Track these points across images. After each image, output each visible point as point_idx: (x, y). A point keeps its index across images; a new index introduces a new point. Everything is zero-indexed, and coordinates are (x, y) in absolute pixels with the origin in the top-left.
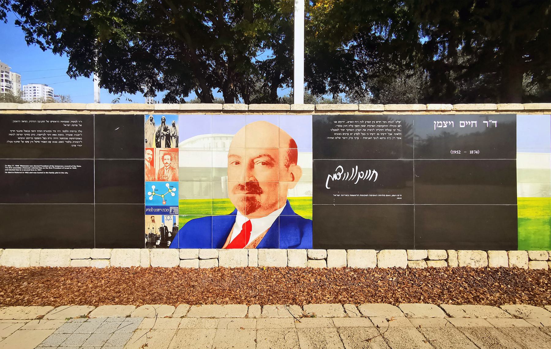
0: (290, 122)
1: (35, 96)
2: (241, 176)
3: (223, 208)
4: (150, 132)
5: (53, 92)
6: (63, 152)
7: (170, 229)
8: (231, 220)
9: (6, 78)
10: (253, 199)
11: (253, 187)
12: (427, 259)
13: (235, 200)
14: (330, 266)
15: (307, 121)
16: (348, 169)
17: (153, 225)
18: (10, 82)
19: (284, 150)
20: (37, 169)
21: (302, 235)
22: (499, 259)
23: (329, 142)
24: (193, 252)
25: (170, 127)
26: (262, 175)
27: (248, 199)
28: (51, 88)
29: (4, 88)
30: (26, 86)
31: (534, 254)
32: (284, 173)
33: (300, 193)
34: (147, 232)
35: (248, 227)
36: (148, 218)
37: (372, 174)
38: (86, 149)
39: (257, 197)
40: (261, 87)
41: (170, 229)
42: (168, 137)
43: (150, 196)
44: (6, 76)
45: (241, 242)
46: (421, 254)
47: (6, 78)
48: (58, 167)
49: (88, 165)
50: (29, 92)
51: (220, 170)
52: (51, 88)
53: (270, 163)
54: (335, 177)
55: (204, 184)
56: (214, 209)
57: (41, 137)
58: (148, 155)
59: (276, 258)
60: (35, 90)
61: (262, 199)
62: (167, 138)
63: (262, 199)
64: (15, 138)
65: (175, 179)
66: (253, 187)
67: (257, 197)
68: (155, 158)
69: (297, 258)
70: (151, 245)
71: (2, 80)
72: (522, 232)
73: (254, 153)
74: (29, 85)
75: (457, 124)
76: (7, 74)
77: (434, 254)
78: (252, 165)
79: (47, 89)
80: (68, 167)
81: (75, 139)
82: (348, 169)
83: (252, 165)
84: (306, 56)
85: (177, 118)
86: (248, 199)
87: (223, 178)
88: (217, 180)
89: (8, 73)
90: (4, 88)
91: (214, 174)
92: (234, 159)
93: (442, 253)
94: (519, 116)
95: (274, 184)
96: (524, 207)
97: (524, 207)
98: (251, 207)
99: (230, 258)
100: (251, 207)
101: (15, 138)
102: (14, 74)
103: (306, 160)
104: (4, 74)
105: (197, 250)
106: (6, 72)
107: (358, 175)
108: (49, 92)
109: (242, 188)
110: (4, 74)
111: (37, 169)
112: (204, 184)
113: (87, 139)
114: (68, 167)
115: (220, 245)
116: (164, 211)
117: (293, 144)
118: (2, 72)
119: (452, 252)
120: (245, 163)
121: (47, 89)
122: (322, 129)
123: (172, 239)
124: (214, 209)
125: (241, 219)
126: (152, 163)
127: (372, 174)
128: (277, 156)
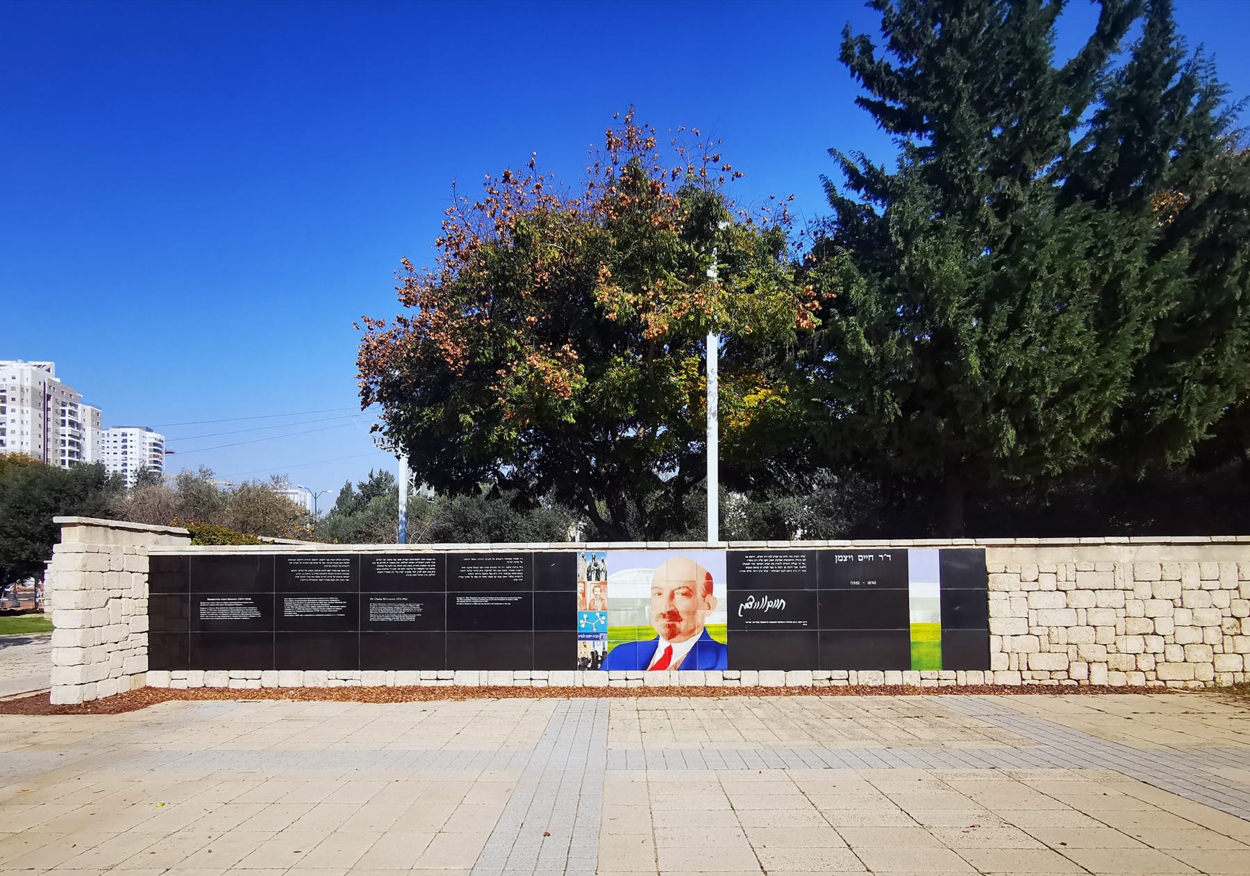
0: (705, 559)
1: (125, 453)
2: (663, 606)
3: (648, 635)
4: (582, 567)
5: (164, 445)
6: (505, 586)
7: (600, 654)
8: (654, 645)
9: (72, 418)
10: (674, 626)
11: (673, 616)
12: (830, 679)
13: (659, 627)
14: (743, 685)
15: (722, 555)
16: (758, 599)
17: (584, 650)
18: (79, 426)
19: (701, 581)
20: (484, 600)
21: (717, 658)
22: (894, 677)
23: (741, 577)
24: (621, 674)
25: (600, 563)
26: (681, 604)
27: (669, 626)
28: (158, 436)
29: (67, 438)
30: (105, 432)
31: (925, 673)
32: (701, 603)
33: (716, 619)
34: (580, 656)
35: (669, 651)
36: (580, 643)
37: (780, 603)
38: (525, 584)
39: (677, 624)
40: (677, 521)
41: (600, 654)
42: (598, 572)
43: (582, 623)
44: (71, 412)
45: (664, 664)
46: (825, 674)
47: (72, 418)
48: (502, 599)
49: (527, 597)
50: (112, 444)
51: (644, 600)
52: (158, 436)
53: (689, 594)
54: (747, 606)
55: (630, 613)
56: (639, 635)
57: (488, 573)
58: (580, 587)
59: (696, 678)
60: (125, 441)
61: (681, 626)
62: (596, 573)
63: (681, 626)
64: (466, 574)
65: (604, 609)
66: (673, 616)
67: (677, 624)
68: (586, 591)
69: (714, 678)
70: (583, 668)
71: (64, 421)
72: (914, 653)
73: (674, 586)
74: (113, 431)
75: (856, 558)
76: (73, 408)
77: (837, 674)
78: (672, 596)
79: (151, 437)
80: (510, 599)
81: (517, 575)
82: (758, 599)
83: (672, 596)
84: (720, 462)
85: (605, 555)
86: (669, 626)
87: (647, 608)
88: (642, 609)
89: (76, 406)
90: (67, 438)
91: (639, 604)
92: (656, 591)
93: (844, 673)
94: (910, 550)
95: (692, 613)
96: (916, 632)
97: (916, 632)
98: (673, 633)
99: (653, 678)
100: (673, 633)
101: (466, 574)
102: (89, 408)
103: (721, 590)
104: (67, 409)
105: (624, 672)
106: (71, 404)
107: (768, 604)
108: (155, 444)
109: (664, 616)
110: (67, 409)
111: (484, 600)
112: (630, 613)
113: (527, 574)
114: (510, 599)
115: (644, 668)
116: (594, 637)
117: (709, 577)
118: (64, 404)
119: (852, 672)
120: (666, 594)
121: (151, 437)
122: (735, 560)
123: (601, 662)
124: (639, 635)
125: (663, 644)
126: (584, 595)
127: (780, 603)
128: (694, 588)
